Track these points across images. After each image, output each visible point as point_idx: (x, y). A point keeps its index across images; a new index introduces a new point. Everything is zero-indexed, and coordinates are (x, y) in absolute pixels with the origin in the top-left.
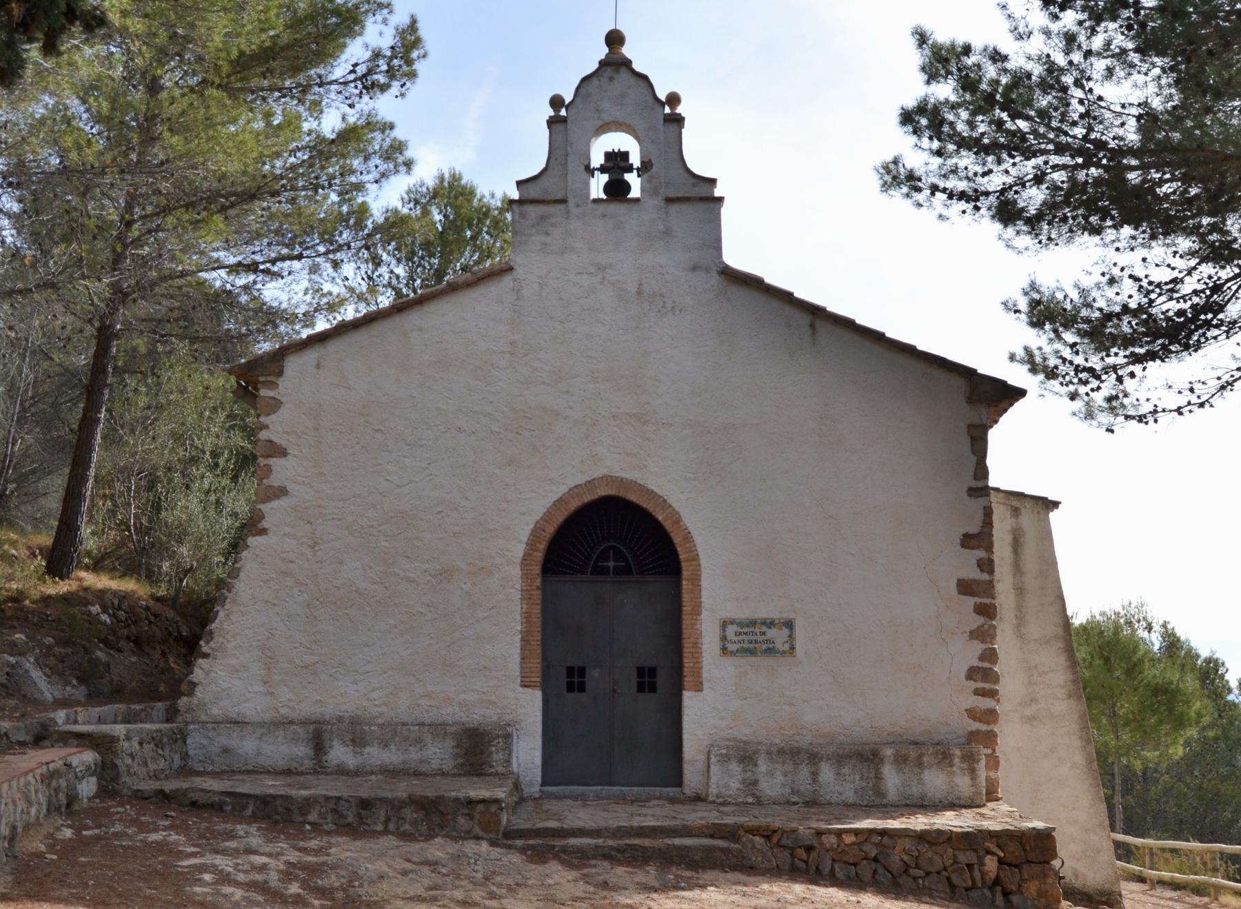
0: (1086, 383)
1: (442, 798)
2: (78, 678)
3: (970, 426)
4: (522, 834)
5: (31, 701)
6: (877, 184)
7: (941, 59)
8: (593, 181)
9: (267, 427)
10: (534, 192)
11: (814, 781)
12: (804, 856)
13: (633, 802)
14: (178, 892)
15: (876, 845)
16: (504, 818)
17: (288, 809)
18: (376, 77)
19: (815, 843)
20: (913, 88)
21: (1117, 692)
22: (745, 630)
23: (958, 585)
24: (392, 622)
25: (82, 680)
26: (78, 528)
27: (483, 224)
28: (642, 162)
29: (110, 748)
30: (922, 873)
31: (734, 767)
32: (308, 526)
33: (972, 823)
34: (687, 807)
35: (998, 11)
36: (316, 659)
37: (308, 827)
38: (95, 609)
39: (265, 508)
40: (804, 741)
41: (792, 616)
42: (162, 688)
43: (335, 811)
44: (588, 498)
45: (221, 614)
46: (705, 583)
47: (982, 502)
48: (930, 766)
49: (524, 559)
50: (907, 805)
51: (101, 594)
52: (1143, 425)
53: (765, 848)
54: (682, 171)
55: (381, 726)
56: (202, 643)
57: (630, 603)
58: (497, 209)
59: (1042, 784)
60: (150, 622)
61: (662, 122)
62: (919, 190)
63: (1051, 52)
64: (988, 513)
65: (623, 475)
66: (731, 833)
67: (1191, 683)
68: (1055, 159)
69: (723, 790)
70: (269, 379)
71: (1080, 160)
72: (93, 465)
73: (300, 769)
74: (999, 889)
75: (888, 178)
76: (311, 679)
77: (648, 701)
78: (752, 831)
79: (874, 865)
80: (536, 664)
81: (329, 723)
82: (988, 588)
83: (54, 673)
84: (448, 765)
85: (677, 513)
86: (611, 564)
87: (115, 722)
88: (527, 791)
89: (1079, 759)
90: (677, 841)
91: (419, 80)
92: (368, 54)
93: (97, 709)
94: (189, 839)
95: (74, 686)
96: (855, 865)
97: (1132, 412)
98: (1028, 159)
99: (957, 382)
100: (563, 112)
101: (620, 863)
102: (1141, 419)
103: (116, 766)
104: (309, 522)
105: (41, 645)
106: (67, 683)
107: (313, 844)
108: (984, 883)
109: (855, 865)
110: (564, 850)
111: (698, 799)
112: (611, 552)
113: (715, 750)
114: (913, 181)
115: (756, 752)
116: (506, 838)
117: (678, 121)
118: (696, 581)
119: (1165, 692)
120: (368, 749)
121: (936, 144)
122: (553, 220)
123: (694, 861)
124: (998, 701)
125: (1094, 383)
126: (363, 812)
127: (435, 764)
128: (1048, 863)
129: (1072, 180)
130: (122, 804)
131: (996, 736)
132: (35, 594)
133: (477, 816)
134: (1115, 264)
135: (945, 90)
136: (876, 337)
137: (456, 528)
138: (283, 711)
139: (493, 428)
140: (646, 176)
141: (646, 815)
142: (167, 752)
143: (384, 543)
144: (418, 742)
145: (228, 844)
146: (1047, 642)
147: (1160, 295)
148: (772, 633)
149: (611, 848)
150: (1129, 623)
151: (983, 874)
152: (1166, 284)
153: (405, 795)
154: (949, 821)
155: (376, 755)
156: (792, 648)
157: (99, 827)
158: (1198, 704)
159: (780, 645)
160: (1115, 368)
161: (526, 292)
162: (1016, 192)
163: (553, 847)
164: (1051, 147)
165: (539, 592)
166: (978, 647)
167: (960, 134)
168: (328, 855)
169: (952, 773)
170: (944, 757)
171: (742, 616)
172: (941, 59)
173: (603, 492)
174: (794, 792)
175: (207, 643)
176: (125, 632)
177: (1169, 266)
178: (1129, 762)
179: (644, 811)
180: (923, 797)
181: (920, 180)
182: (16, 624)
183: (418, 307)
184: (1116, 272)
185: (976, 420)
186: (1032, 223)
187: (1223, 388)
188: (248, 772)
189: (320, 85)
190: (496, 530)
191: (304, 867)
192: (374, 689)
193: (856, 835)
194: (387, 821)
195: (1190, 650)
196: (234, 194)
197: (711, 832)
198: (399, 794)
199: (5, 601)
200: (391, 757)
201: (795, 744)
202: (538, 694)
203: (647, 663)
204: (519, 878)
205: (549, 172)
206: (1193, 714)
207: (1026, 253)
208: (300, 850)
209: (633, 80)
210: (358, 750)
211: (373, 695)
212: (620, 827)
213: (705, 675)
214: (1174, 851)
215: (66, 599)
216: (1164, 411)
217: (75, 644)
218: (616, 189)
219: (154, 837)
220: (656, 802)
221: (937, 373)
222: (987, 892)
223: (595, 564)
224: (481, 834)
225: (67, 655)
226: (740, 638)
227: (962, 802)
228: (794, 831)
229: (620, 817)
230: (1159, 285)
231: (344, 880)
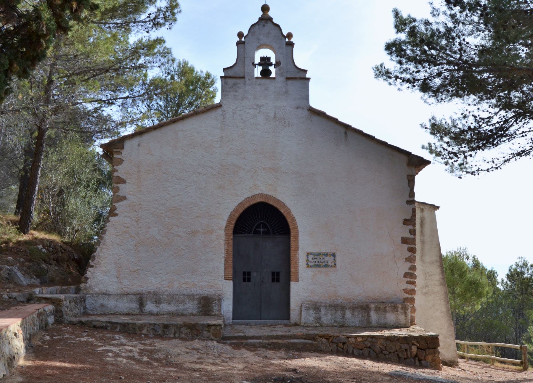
0: (452, 158)
1: (197, 325)
2: (36, 275)
3: (408, 175)
5: (18, 285)
6: (374, 74)
7: (401, 23)
8: (256, 69)
9: (117, 171)
10: (231, 73)
11: (343, 317)
12: (342, 346)
13: (270, 326)
14: (101, 360)
15: (370, 342)
17: (134, 329)
18: (159, 20)
19: (346, 341)
20: (392, 35)
21: (456, 283)
22: (316, 257)
25: (38, 276)
26: (31, 212)
27: (198, 84)
28: (276, 62)
29: (59, 304)
30: (388, 353)
31: (312, 312)
33: (406, 333)
35: (429, 5)
36: (139, 268)
37: (143, 336)
38: (40, 247)
40: (339, 302)
41: (335, 251)
42: (69, 280)
43: (153, 329)
44: (252, 203)
45: (98, 249)
47: (412, 206)
48: (389, 312)
49: (226, 228)
50: (379, 327)
51: (42, 241)
52: (473, 176)
54: (293, 66)
55: (167, 295)
56: (90, 261)
57: (269, 246)
58: (204, 78)
59: (431, 317)
60: (62, 253)
61: (285, 45)
62: (390, 78)
63: (447, 22)
64: (414, 211)
65: (267, 193)
66: (313, 338)
67: (484, 280)
68: (446, 67)
70: (118, 150)
71: (456, 68)
72: (37, 186)
73: (134, 313)
74: (417, 358)
75: (378, 72)
76: (137, 276)
78: (322, 337)
79: (369, 349)
80: (230, 271)
81: (145, 294)
82: (413, 241)
83: (26, 273)
84: (195, 311)
87: (56, 294)
89: (444, 309)
90: (292, 341)
91: (177, 22)
92: (156, 10)
93: (50, 288)
94: (97, 340)
95: (35, 279)
96: (362, 349)
97: (469, 170)
98: (435, 66)
99: (404, 158)
100: (243, 39)
101: (270, 349)
102: (473, 173)
103: (61, 311)
105: (19, 262)
106: (32, 278)
107: (147, 342)
108: (411, 356)
109: (362, 349)
110: (247, 344)
111: (296, 325)
112: (262, 226)
113: (304, 306)
114: (388, 74)
115: (320, 306)
116: (223, 339)
117: (291, 45)
118: (296, 237)
119: (474, 283)
120: (162, 305)
121: (398, 59)
122: (239, 85)
123: (299, 349)
124: (416, 286)
125: (455, 159)
126: (165, 330)
127: (190, 311)
128: (436, 348)
129: (453, 76)
130: (65, 327)
131: (414, 299)
132: (14, 240)
133: (212, 331)
134: (467, 110)
135: (403, 36)
136: (372, 138)
137: (198, 214)
138: (125, 289)
139: (213, 173)
140: (278, 68)
142: (79, 306)
144: (183, 302)
145: (114, 342)
146: (433, 263)
147: (483, 123)
148: (327, 258)
149: (266, 343)
150: (460, 256)
151: (411, 353)
152: (486, 119)
153: (182, 323)
154: (397, 332)
155: (165, 307)
156: (335, 265)
157: (60, 335)
158: (487, 288)
160: (464, 152)
161: (227, 116)
162: (430, 80)
163: (243, 343)
164: (444, 61)
166: (409, 265)
167: (408, 55)
168: (155, 346)
169: (398, 314)
170: (395, 308)
172: (401, 23)
173: (259, 200)
174: (335, 322)
175: (93, 261)
176: (52, 256)
177: (488, 111)
178: (459, 311)
179: (276, 329)
180: (386, 323)
181: (391, 73)
182: (7, 253)
183: (181, 121)
184: (467, 113)
185: (411, 174)
186: (436, 92)
187: (505, 161)
188: (112, 314)
189: (134, 23)
191: (147, 351)
192: (164, 280)
193: (362, 338)
194: (175, 333)
195: (483, 267)
196: (98, 70)
197: (305, 337)
198: (179, 322)
199: (2, 243)
200: (172, 308)
201: (335, 303)
202: (231, 283)
204: (232, 355)
205: (237, 65)
206: (485, 292)
207: (432, 105)
208: (143, 344)
209: (273, 27)
210: (158, 305)
211: (163, 283)
213: (300, 275)
214: (476, 346)
215: (26, 242)
216: (482, 170)
217: (33, 261)
218: (266, 73)
219: (83, 339)
220: (280, 326)
221: (389, 151)
222: (412, 360)
223: (255, 230)
224: (213, 338)
225: (31, 266)
226: (314, 260)
227: (401, 326)
228: (338, 337)
229: (267, 332)
230: (483, 119)
231: (164, 356)
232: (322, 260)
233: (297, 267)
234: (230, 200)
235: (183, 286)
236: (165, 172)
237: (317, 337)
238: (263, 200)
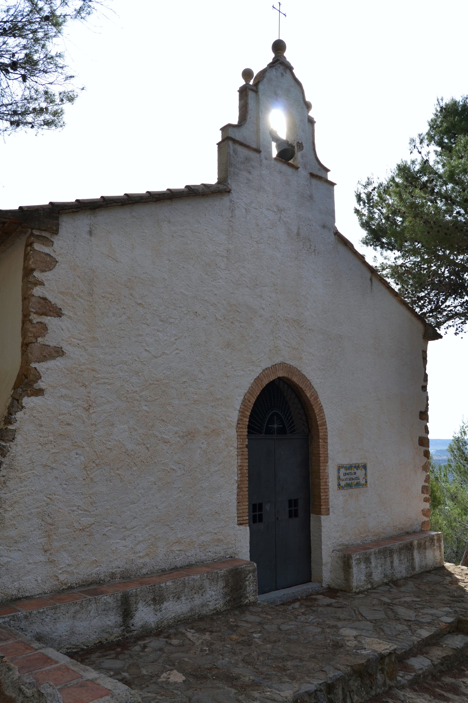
9: (42, 284)
11: (392, 566)
22: (348, 472)
23: (419, 440)
24: (153, 479)
32: (83, 388)
36: (92, 520)
39: (41, 367)
54: (313, 157)
65: (291, 364)
85: (316, 392)
104: (85, 386)
120: (166, 604)
138: (62, 578)
143: (145, 408)
156: (366, 482)
159: (363, 482)
174: (386, 576)
192: (140, 542)
209: (293, 82)
213: (330, 504)
226: (347, 476)
232: (354, 476)
234: (243, 371)
235: (173, 548)
236: (140, 301)
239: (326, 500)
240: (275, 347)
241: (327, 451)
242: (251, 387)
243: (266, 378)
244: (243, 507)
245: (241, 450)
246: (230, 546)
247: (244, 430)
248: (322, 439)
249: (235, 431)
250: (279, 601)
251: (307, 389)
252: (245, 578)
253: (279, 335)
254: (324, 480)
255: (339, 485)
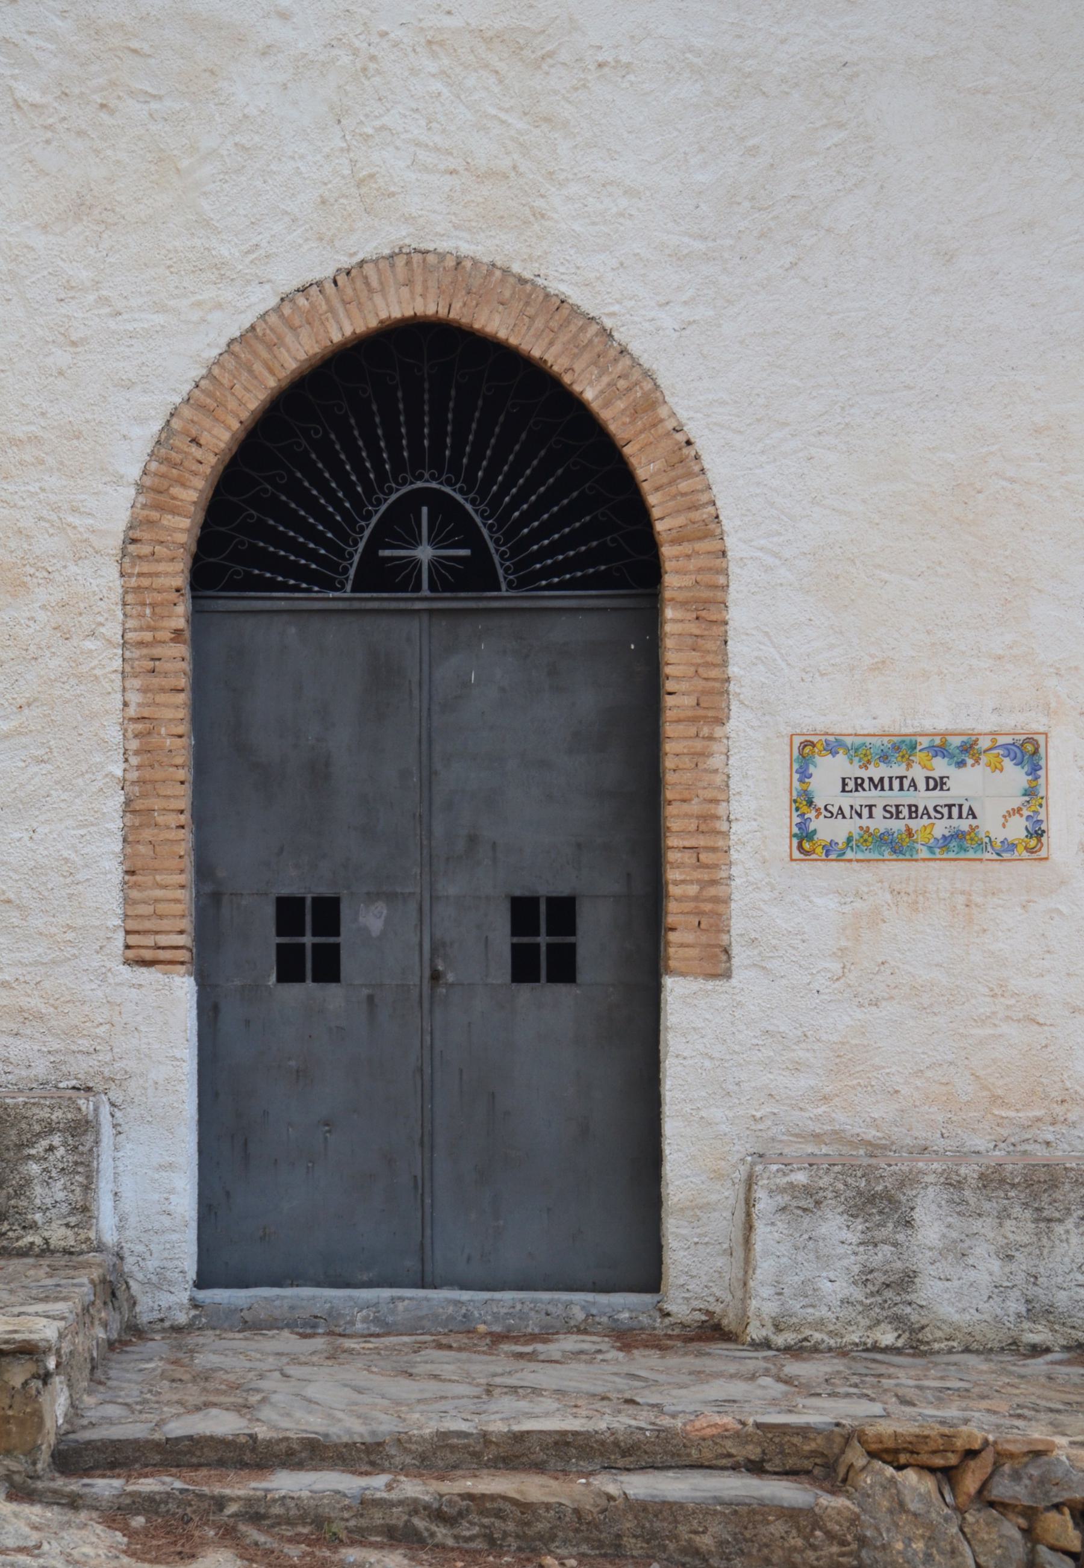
4: (118, 1457)
16: (57, 1405)
31: (835, 1228)
34: (673, 1361)
41: (1035, 723)
44: (344, 327)
46: (741, 613)
53: (938, 1511)
57: (495, 683)
65: (466, 248)
69: (796, 1305)
77: (550, 1012)
78: (894, 1454)
80: (175, 894)
85: (647, 374)
86: (425, 553)
88: (149, 1305)
90: (640, 1486)
110: (256, 1513)
111: (713, 1331)
113: (770, 1176)
115: (907, 1181)
118: (711, 606)
139: (22, 90)
141: (536, 1391)
148: (966, 783)
149: (414, 1507)
156: (1038, 833)
163: (220, 1503)
165: (183, 650)
171: (868, 726)
173: (395, 305)
174: (1035, 1311)
190: (35, 440)
197: (753, 1452)
201: (1041, 1153)
202: (183, 989)
203: (546, 886)
212: (445, 1435)
213: (738, 925)
220: (570, 1343)
226: (860, 798)
232: (925, 799)
233: (712, 858)
234: (161, 308)
237: (856, 1456)
238: (427, 306)
239: (708, 907)
240: (359, 184)
241: (725, 664)
242: (209, 375)
243: (304, 332)
244: (159, 893)
245: (145, 651)
246: (85, 1044)
247: (170, 567)
248: (684, 604)
249: (113, 571)
250: (365, 1320)
251: (578, 366)
252: (20, 1146)
253: (385, 120)
254: (695, 807)
255: (803, 837)
